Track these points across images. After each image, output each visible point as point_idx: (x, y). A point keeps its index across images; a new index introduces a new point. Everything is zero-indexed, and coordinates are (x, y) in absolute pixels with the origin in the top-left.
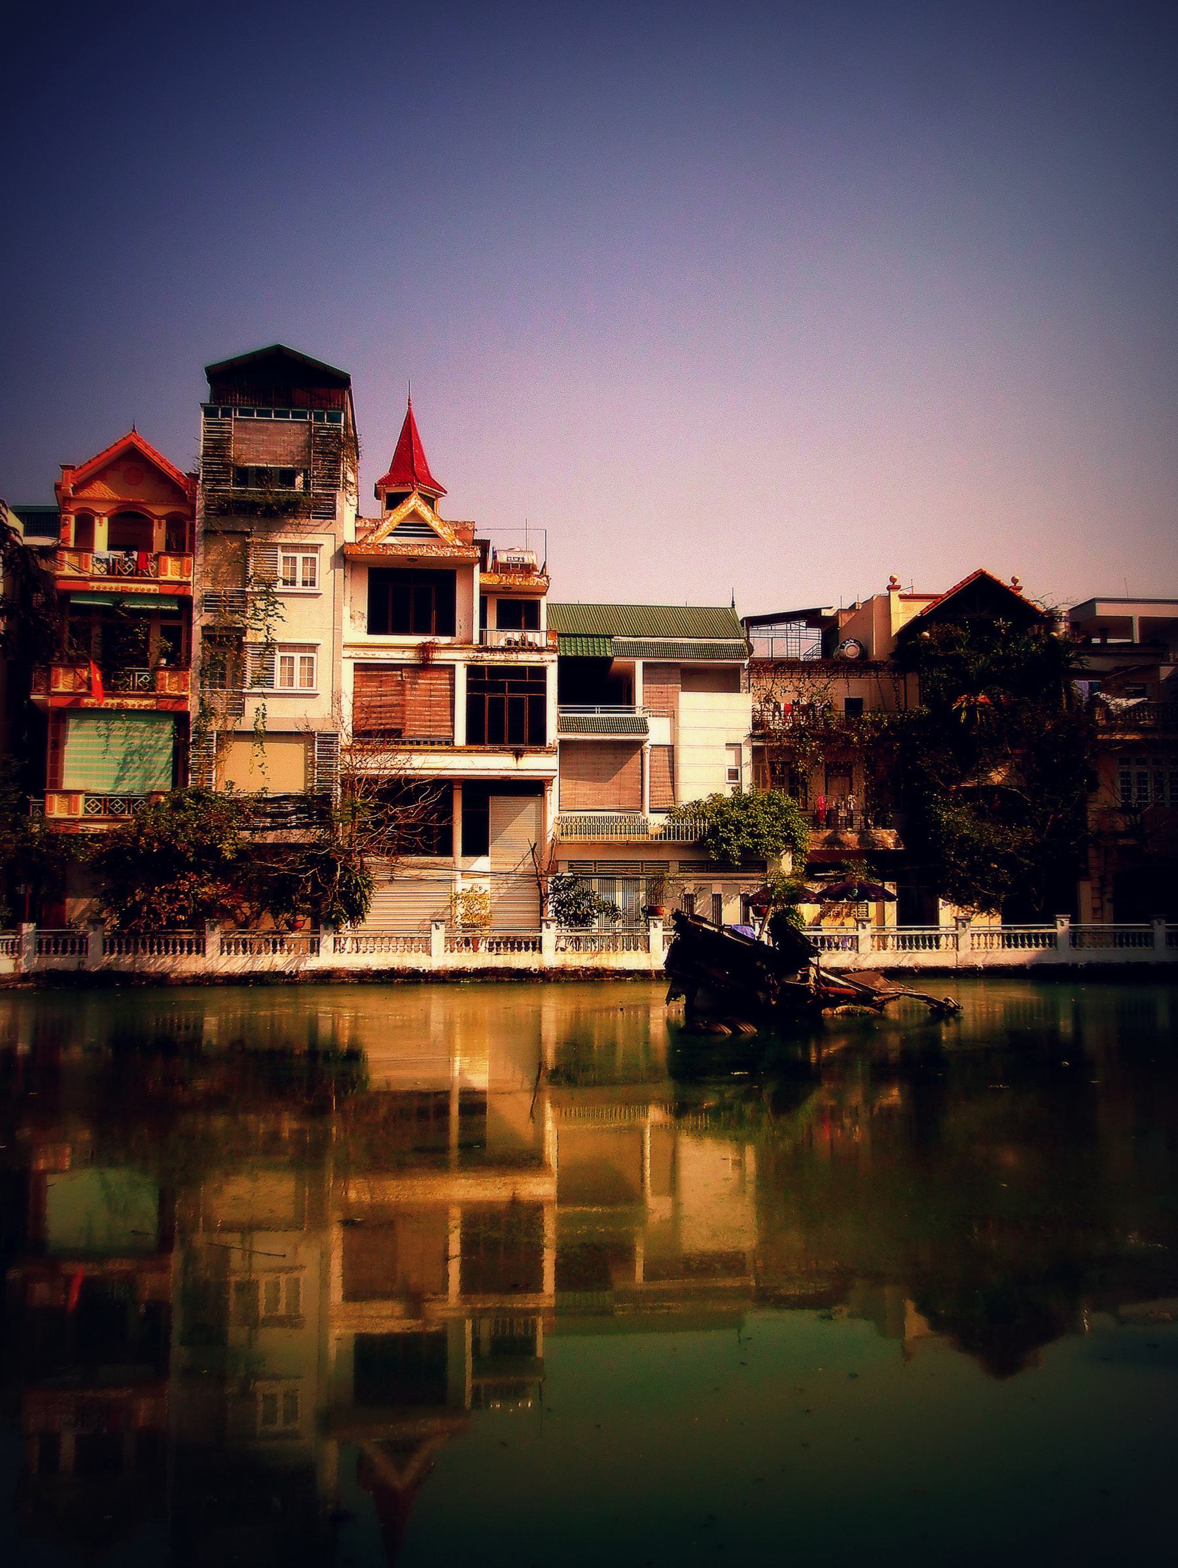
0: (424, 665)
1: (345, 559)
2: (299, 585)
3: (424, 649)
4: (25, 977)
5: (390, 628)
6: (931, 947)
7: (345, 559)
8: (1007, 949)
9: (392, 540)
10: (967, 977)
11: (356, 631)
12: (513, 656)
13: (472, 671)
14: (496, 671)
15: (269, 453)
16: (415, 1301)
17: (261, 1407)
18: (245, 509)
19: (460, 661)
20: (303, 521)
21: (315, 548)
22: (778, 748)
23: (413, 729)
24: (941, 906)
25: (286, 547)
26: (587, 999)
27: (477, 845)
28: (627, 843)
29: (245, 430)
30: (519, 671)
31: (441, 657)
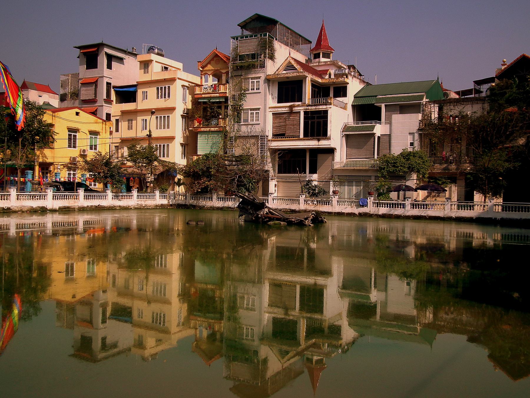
0: (291, 112)
1: (269, 81)
2: (250, 90)
3: (291, 107)
4: (171, 205)
6: (470, 210)
7: (269, 81)
9: (284, 72)
10: (447, 221)
12: (318, 107)
13: (306, 113)
14: (313, 112)
15: (248, 49)
16: (286, 309)
17: (245, 330)
18: (241, 68)
19: (301, 110)
20: (257, 69)
21: (259, 78)
22: (427, 134)
23: (288, 133)
24: (475, 194)
25: (252, 78)
26: (383, 225)
27: (313, 171)
28: (354, 170)
29: (242, 43)
30: (319, 112)
31: (296, 109)
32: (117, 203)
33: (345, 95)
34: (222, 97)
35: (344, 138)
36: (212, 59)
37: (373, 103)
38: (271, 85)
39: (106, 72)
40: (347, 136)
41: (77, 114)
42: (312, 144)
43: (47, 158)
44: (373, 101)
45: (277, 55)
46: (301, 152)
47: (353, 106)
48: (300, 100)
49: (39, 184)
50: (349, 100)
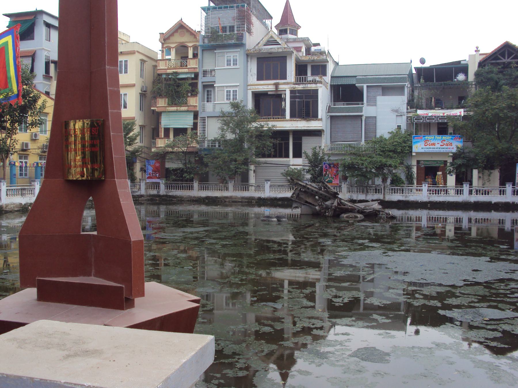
5: (272, 77)
8: (484, 195)
11: (253, 78)
13: (292, 92)
14: (299, 91)
33: (325, 74)
34: (191, 73)
36: (176, 31)
37: (354, 83)
38: (249, 60)
40: (332, 117)
42: (301, 125)
45: (254, 29)
46: (284, 134)
47: (331, 85)
50: (328, 79)
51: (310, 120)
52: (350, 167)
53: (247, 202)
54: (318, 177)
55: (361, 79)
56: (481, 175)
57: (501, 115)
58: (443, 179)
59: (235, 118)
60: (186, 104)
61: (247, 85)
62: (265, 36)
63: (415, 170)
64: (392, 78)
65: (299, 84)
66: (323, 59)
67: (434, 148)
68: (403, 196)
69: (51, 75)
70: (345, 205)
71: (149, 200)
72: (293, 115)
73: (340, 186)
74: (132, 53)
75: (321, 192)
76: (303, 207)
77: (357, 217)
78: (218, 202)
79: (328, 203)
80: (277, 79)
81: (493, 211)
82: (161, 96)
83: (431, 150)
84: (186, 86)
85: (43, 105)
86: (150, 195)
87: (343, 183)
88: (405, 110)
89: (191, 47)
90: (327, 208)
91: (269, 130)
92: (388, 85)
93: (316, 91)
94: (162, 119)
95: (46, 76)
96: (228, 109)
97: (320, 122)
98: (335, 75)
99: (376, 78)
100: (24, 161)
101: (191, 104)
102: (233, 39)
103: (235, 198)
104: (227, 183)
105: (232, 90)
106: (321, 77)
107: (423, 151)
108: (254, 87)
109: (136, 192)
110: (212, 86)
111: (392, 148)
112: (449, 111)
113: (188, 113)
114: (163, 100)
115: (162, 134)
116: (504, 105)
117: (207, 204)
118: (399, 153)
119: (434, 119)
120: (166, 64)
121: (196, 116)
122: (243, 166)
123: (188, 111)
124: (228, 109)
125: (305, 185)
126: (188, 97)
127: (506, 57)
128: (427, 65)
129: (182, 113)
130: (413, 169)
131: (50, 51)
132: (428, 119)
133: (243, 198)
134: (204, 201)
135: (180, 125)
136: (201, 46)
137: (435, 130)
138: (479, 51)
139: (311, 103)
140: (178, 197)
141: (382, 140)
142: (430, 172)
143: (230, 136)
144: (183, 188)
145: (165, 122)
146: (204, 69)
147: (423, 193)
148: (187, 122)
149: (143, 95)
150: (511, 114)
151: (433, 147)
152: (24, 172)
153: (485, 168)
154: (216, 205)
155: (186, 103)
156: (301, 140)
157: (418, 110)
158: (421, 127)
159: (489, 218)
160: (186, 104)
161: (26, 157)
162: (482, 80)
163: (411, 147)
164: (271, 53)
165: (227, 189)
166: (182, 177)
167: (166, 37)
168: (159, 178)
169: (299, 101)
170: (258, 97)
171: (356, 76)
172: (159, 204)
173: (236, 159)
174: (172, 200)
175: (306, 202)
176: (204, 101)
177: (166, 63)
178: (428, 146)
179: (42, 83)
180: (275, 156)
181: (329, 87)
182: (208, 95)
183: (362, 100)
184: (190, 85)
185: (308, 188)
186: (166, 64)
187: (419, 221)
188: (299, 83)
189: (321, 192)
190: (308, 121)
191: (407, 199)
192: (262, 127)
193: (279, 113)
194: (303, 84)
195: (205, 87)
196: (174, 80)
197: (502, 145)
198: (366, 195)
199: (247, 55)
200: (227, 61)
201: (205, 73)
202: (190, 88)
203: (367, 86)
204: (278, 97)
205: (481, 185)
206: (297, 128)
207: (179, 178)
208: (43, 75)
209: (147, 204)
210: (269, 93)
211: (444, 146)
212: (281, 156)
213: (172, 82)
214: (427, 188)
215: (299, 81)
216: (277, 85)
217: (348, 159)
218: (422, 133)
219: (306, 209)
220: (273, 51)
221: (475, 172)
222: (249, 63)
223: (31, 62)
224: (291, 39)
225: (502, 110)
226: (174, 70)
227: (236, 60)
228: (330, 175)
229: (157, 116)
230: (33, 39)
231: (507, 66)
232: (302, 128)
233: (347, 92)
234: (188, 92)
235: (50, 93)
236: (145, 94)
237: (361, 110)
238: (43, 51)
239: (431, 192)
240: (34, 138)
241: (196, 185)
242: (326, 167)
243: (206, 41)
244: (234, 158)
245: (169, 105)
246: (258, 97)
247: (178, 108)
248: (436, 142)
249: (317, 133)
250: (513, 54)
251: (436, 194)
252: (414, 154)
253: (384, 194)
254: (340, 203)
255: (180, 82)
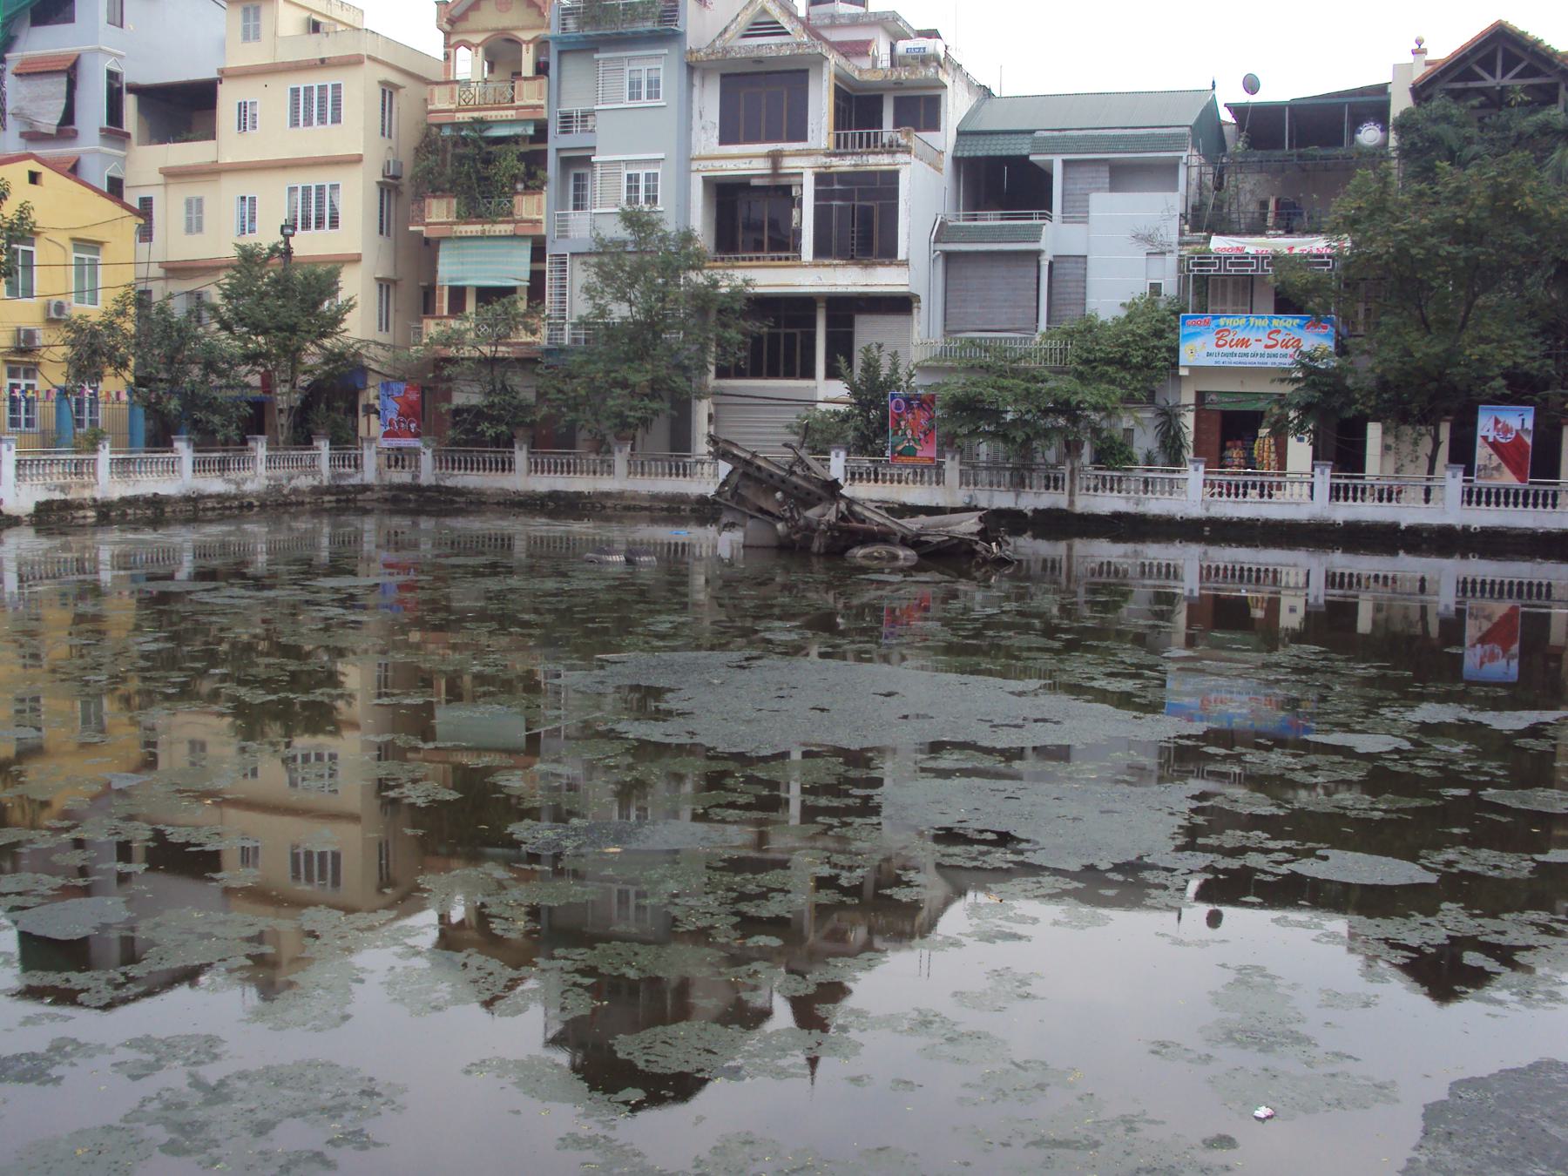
11: (706, 138)
13: (820, 178)
14: (843, 177)
32: (214, 485)
33: (933, 124)
34: (525, 122)
35: (940, 263)
37: (1025, 152)
38: (697, 81)
39: (108, 38)
40: (949, 257)
41: (34, 178)
43: (1273, 920)
44: (1021, 147)
46: (797, 308)
47: (957, 161)
48: (801, 136)
49: (421, 723)
50: (945, 139)
51: (873, 265)
52: (970, 409)
53: (667, 509)
54: (876, 436)
55: (1045, 138)
56: (1391, 441)
57: (1414, 251)
58: (1277, 452)
59: (640, 256)
60: (509, 215)
61: (688, 159)
62: (745, 8)
63: (1188, 421)
64: (1142, 136)
65: (841, 155)
66: (926, 78)
67: (1246, 355)
68: (1128, 499)
69: (126, 128)
70: (863, 521)
71: (386, 500)
72: (823, 250)
73: (940, 466)
74: (354, 61)
75: (794, 479)
76: (750, 523)
77: (895, 557)
78: (584, 508)
79: (812, 513)
80: (778, 139)
81: (1401, 553)
82: (437, 191)
83: (1234, 362)
84: (511, 162)
85: (21, 218)
86: (392, 487)
87: (948, 456)
88: (1175, 237)
89: (528, 42)
90: (810, 528)
91: (735, 294)
92: (1128, 162)
93: (892, 177)
94: (441, 261)
95: (109, 131)
96: (616, 230)
97: (903, 270)
98: (968, 129)
99: (1093, 137)
100: (23, 382)
101: (525, 216)
102: (647, 19)
103: (633, 498)
104: (609, 452)
105: (642, 172)
106: (908, 134)
107: (1210, 362)
108: (708, 163)
109: (349, 476)
110: (586, 161)
111: (1116, 353)
112: (1308, 239)
113: (515, 243)
114: (444, 203)
115: (443, 305)
116: (1424, 221)
117: (554, 515)
118: (1139, 368)
119: (1250, 264)
120: (452, 97)
121: (538, 253)
122: (647, 401)
123: (514, 237)
124: (616, 230)
125: (748, 457)
126: (517, 193)
127: (1499, 72)
128: (1264, 96)
129: (465, 244)
130: (1182, 419)
131: (121, 57)
132: (1232, 264)
133: (655, 497)
134: (542, 505)
135: (495, 278)
136: (554, 38)
137: (1267, 301)
138: (1424, 52)
139: (876, 213)
140: (470, 492)
141: (1089, 328)
142: (1233, 430)
143: (620, 311)
144: (485, 466)
145: (451, 269)
146: (566, 108)
147: (1191, 493)
148: (512, 268)
149: (389, 188)
150: (1450, 249)
151: (1243, 350)
152: (23, 416)
153: (1404, 418)
154: (579, 518)
155: (511, 214)
156: (851, 325)
157: (1214, 238)
158: (1212, 288)
159: (1390, 575)
160: (509, 215)
161: (31, 370)
162: (1413, 144)
163: (1174, 351)
164: (759, 61)
165: (610, 470)
166: (473, 431)
167: (456, 13)
168: (416, 435)
169: (840, 207)
170: (727, 196)
171: (1032, 132)
172: (417, 512)
173: (626, 379)
174: (453, 502)
175: (761, 510)
176: (564, 207)
177: (452, 90)
178: (1226, 349)
179: (97, 151)
180: (756, 373)
181: (947, 163)
182: (577, 188)
183: (1047, 204)
184: (522, 157)
185: (759, 468)
186: (452, 97)
187: (1176, 577)
188: (842, 150)
189: (794, 479)
190: (866, 266)
191: (1141, 509)
192: (715, 284)
193: (783, 244)
194: (853, 154)
195: (566, 163)
196: (474, 141)
197: (1426, 348)
198: (1017, 496)
199: (691, 68)
200: (631, 85)
201: (567, 121)
202: (522, 167)
203: (1065, 162)
204: (781, 193)
205: (1390, 471)
206: (833, 290)
207: (480, 435)
208: (102, 130)
209: (383, 511)
210: (755, 182)
211: (1277, 350)
212: (790, 374)
213: (470, 150)
214: (1201, 475)
215: (841, 147)
216: (775, 157)
217: (956, 385)
218: (1229, 306)
219: (755, 530)
220: (765, 53)
221: (1374, 431)
222: (696, 92)
223: (64, 88)
224: (843, 16)
225: (1418, 237)
226: (476, 114)
227: (658, 82)
228: (909, 432)
229: (428, 249)
230: (71, 20)
231: (1497, 100)
232: (850, 290)
233: (1005, 180)
234: (515, 178)
235: (125, 183)
236: (396, 187)
237: (1035, 234)
238: (100, 56)
239: (1216, 490)
240: (54, 315)
241: (521, 456)
242: (898, 407)
243: (571, 24)
244: (619, 376)
245: (463, 218)
246: (727, 196)
247: (487, 227)
248: (1252, 336)
249: (901, 304)
250: (1519, 61)
251: (1229, 495)
252: (1183, 372)
253: (1071, 494)
254: (850, 515)
255: (493, 148)
